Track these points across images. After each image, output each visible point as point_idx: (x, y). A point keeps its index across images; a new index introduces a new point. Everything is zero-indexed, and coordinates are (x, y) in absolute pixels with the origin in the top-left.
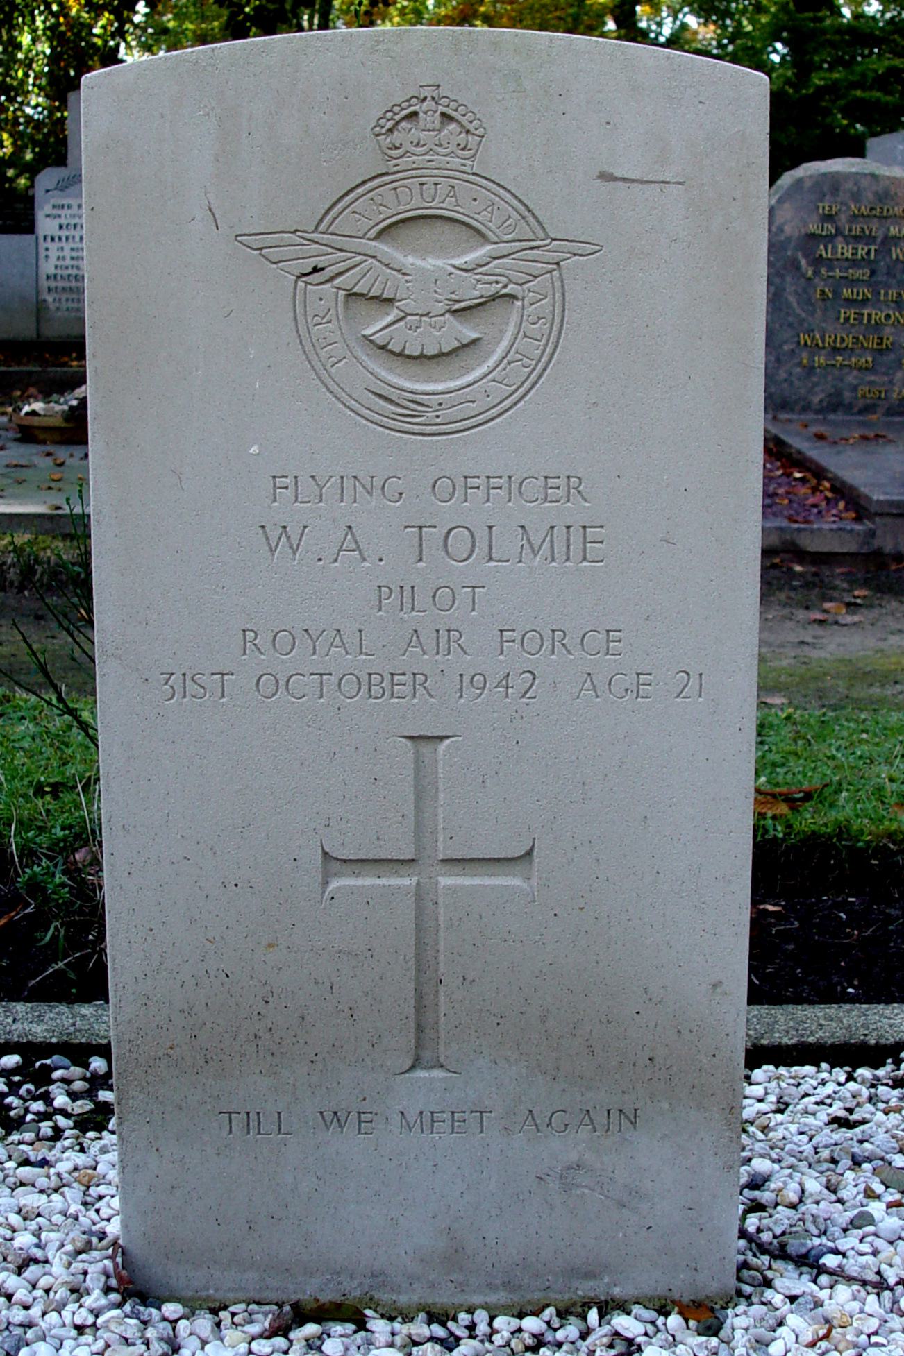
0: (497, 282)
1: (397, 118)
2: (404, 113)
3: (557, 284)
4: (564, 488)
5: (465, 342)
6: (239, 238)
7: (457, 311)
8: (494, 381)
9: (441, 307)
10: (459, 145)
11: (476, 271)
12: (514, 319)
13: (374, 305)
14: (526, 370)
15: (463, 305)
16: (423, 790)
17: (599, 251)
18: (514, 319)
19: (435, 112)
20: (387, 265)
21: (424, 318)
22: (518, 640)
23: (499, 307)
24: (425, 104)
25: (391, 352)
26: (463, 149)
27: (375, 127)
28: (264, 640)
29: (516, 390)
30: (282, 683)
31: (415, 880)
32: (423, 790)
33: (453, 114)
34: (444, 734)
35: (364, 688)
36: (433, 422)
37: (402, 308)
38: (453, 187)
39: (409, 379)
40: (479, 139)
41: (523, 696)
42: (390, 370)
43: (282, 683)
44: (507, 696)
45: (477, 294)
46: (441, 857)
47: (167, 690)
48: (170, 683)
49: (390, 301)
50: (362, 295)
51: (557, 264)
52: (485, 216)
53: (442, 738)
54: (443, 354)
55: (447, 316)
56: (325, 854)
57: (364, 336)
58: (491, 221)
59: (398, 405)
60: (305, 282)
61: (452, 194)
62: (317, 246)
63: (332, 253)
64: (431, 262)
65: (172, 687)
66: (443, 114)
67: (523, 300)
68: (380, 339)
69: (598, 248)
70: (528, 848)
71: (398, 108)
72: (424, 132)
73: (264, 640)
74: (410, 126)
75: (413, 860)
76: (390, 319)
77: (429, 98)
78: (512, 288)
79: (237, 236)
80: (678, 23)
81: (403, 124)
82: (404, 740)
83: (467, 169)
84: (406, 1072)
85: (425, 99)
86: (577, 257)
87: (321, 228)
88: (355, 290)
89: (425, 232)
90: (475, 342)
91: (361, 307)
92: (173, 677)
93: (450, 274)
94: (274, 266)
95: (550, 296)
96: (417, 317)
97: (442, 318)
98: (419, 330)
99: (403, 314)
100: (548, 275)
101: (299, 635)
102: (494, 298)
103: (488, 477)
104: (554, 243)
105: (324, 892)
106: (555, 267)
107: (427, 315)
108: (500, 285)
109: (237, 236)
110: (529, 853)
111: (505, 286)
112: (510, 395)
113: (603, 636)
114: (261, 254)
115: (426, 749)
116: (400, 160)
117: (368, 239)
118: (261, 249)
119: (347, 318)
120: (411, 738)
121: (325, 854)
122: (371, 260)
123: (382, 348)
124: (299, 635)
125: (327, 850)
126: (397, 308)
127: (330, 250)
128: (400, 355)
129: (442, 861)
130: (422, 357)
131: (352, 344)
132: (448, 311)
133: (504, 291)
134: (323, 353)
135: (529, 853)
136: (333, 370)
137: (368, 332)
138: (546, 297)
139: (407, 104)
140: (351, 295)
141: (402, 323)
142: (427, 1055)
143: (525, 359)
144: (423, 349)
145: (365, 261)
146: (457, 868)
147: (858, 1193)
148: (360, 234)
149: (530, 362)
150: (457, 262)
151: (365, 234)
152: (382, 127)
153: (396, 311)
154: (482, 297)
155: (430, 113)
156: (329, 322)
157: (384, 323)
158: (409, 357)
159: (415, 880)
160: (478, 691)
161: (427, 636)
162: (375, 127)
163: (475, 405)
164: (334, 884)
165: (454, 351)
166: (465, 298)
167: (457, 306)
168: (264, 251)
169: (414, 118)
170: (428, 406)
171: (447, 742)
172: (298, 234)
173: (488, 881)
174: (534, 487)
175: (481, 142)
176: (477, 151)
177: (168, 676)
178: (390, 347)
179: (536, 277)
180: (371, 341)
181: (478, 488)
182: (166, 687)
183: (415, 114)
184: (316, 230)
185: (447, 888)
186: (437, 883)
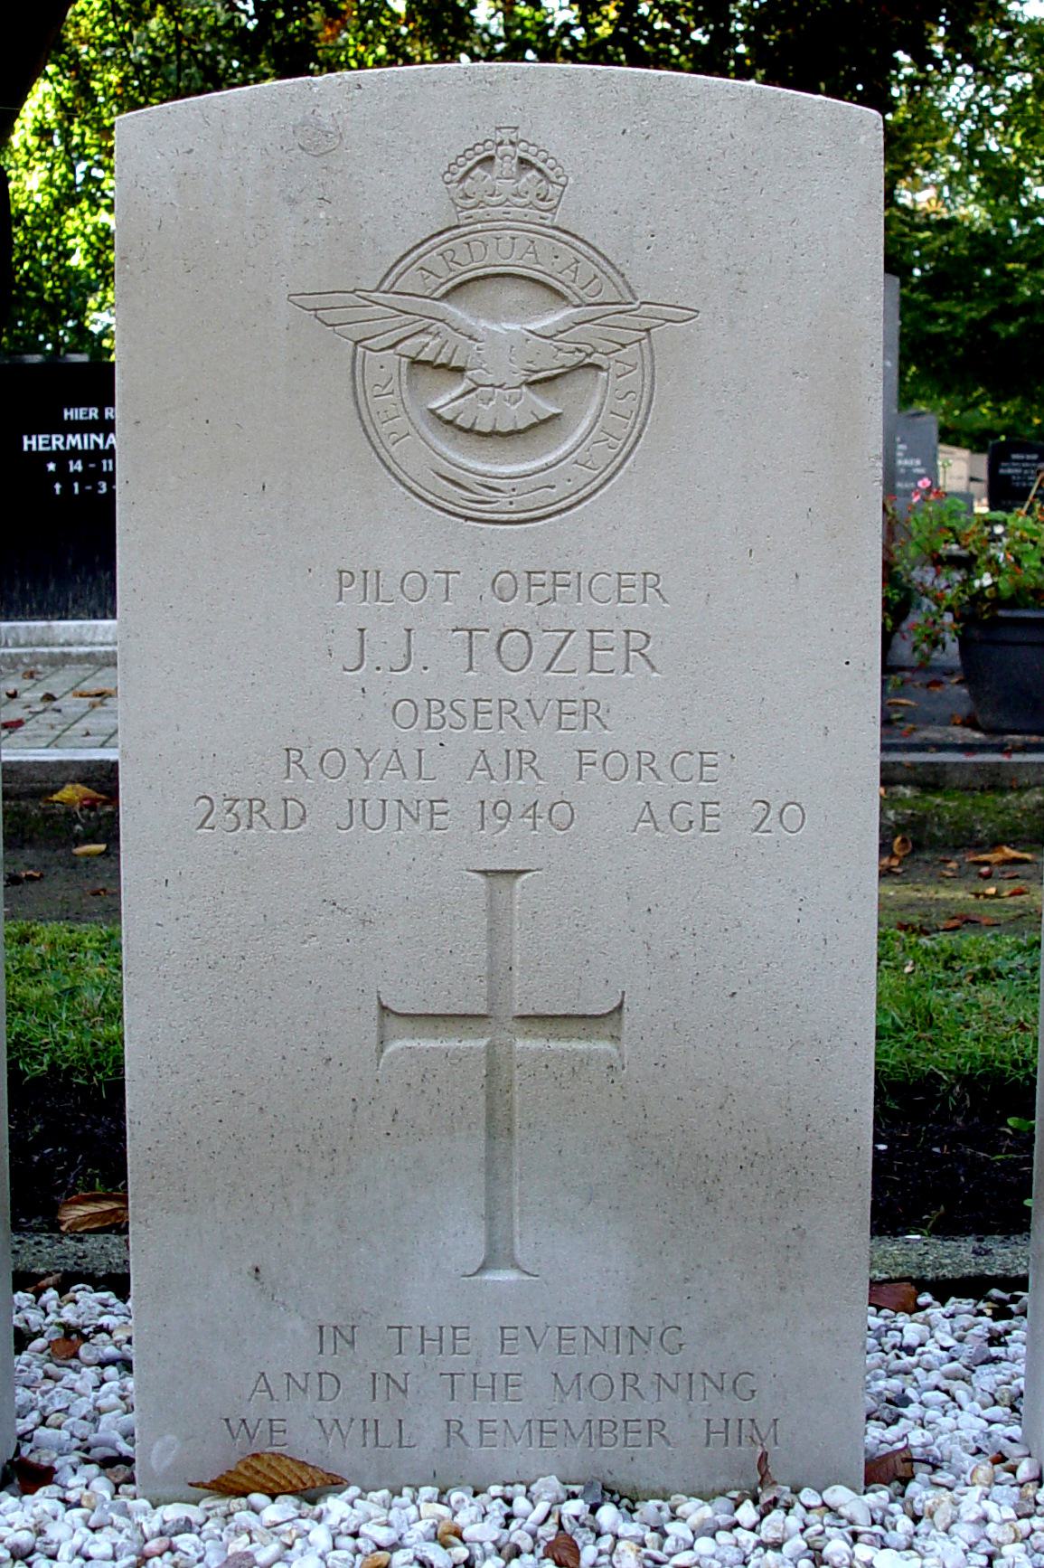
1: (470, 164)
2: (478, 158)
3: (646, 352)
4: (639, 584)
5: (542, 417)
6: (292, 297)
7: (534, 382)
8: (576, 462)
10: (538, 195)
12: (599, 389)
13: (444, 376)
15: (541, 375)
16: (496, 931)
17: (694, 317)
18: (599, 389)
19: (513, 158)
20: (456, 330)
21: (497, 390)
25: (461, 429)
26: (543, 200)
27: (446, 173)
29: (600, 473)
31: (483, 1043)
32: (496, 931)
33: (533, 160)
34: (520, 868)
36: (504, 509)
37: (475, 379)
39: (517, 462)
40: (561, 188)
42: (459, 449)
44: (535, 828)
45: (558, 364)
49: (460, 370)
51: (648, 330)
52: (566, 274)
54: (519, 432)
55: (524, 389)
56: (384, 1008)
57: (432, 411)
58: (574, 281)
59: (471, 492)
60: (364, 347)
61: (531, 249)
65: (235, 815)
66: (522, 161)
67: (607, 370)
68: (446, 413)
69: (695, 314)
70: (615, 1005)
71: (463, 159)
72: (502, 179)
73: (309, 761)
74: (485, 174)
75: (484, 1016)
76: (459, 391)
80: (23, 224)
82: (476, 876)
83: (547, 222)
84: (474, 1274)
86: (668, 324)
87: (382, 289)
88: (422, 357)
90: (556, 416)
91: (427, 376)
93: (527, 340)
96: (490, 389)
97: (518, 390)
99: (473, 386)
102: (580, 367)
103: (555, 573)
106: (644, 334)
107: (500, 387)
108: (583, 354)
110: (620, 1007)
111: (589, 355)
114: (316, 316)
115: (502, 882)
116: (474, 211)
118: (316, 310)
120: (485, 872)
122: (439, 324)
123: (449, 423)
124: (351, 755)
125: (384, 1003)
131: (417, 420)
133: (588, 360)
134: (383, 429)
135: (620, 1007)
136: (393, 449)
137: (434, 405)
139: (471, 152)
140: (415, 362)
144: (516, 423)
146: (536, 1027)
147: (75, 1292)
150: (531, 327)
152: (453, 174)
154: (563, 367)
155: (507, 158)
157: (454, 394)
158: (480, 434)
159: (483, 1043)
160: (503, 822)
162: (446, 173)
163: (554, 490)
164: (392, 1047)
165: (511, 433)
166: (544, 366)
167: (535, 377)
168: (319, 312)
169: (490, 163)
170: (501, 491)
172: (358, 293)
174: (605, 585)
175: (563, 191)
176: (559, 202)
179: (624, 346)
180: (440, 417)
181: (543, 585)
182: (230, 815)
183: (491, 158)
184: (377, 290)
186: (511, 1046)
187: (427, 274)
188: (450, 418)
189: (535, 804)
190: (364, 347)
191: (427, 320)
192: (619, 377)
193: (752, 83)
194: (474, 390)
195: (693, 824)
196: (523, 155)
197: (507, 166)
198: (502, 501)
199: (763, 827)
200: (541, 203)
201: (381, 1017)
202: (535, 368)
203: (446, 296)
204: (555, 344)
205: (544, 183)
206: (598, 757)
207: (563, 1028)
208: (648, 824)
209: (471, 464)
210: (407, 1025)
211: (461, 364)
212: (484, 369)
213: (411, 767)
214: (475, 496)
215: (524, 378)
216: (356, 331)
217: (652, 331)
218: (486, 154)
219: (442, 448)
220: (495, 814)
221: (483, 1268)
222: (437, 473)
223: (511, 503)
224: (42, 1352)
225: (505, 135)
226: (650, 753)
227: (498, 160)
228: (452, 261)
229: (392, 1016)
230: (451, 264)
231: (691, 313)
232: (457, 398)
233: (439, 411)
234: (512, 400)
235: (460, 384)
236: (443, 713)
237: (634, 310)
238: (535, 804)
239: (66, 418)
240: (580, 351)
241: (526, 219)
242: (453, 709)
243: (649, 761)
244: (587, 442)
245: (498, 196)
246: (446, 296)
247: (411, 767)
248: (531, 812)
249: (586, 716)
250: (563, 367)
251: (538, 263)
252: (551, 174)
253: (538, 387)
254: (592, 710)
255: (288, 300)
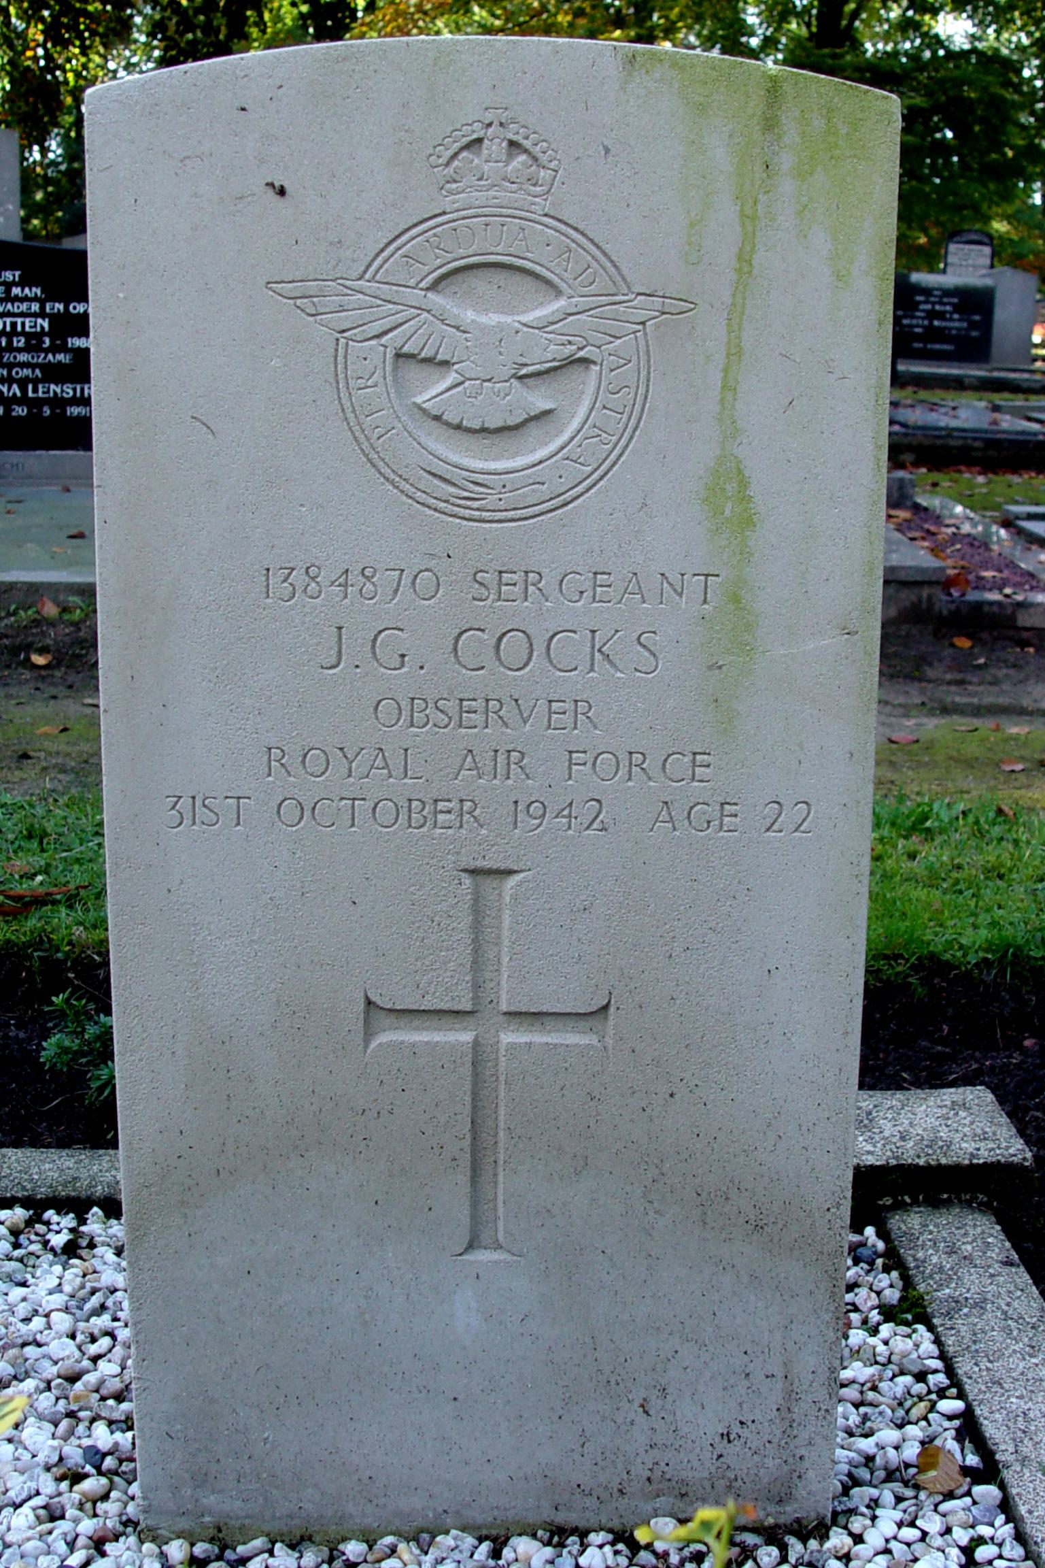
0: (570, 343)
8: (567, 459)
9: (507, 371)
11: (546, 329)
13: (428, 369)
14: (606, 447)
15: (531, 369)
17: (692, 310)
22: (589, 765)
23: (576, 372)
24: (490, 130)
25: (448, 424)
28: (292, 761)
30: (307, 813)
31: (467, 1037)
35: (403, 818)
38: (523, 229)
40: (554, 173)
41: (796, 830)
43: (307, 813)
45: (549, 356)
46: (504, 1007)
47: (173, 815)
48: (177, 807)
49: (446, 364)
50: (412, 356)
51: (643, 323)
53: (510, 872)
56: (369, 1003)
57: (414, 403)
59: (454, 485)
62: (361, 296)
63: (403, 311)
64: (492, 319)
66: (512, 144)
69: (693, 306)
73: (292, 761)
76: (448, 382)
77: (496, 123)
78: (590, 351)
79: (268, 283)
81: (464, 154)
84: (460, 1255)
85: (490, 125)
88: (405, 350)
89: (480, 283)
91: (412, 372)
92: (182, 800)
93: (517, 332)
94: (311, 319)
95: (634, 359)
98: (508, 398)
100: (632, 336)
101: (655, 771)
104: (639, 298)
105: (366, 1047)
106: (640, 327)
108: (575, 347)
109: (268, 283)
110: (606, 1007)
112: (588, 477)
113: (689, 757)
114: (295, 305)
115: (489, 884)
117: (421, 289)
119: (395, 381)
121: (369, 1003)
122: (425, 315)
123: (437, 418)
125: (373, 999)
126: (456, 372)
127: (381, 303)
128: (458, 427)
129: (505, 1014)
130: (483, 430)
132: (514, 376)
133: (581, 354)
135: (606, 1007)
137: (419, 400)
138: (630, 361)
141: (460, 389)
142: (486, 1237)
143: (604, 435)
145: (419, 315)
148: (412, 282)
149: (610, 438)
150: (525, 318)
151: (417, 285)
152: (439, 157)
153: (454, 375)
154: (554, 360)
156: (376, 386)
158: (470, 431)
159: (467, 1037)
161: (485, 760)
167: (524, 371)
169: (477, 146)
170: (488, 487)
171: (513, 881)
172: (339, 281)
173: (437, 1037)
175: (555, 177)
177: (175, 799)
178: (445, 417)
180: (424, 411)
181: (515, 584)
182: (173, 812)
183: (479, 141)
185: (512, 1047)
187: (414, 262)
188: (439, 414)
189: (571, 804)
190: (345, 338)
191: (391, 306)
192: (612, 371)
193: (252, 53)
194: (462, 383)
195: (712, 824)
196: (515, 138)
197: (495, 147)
198: (491, 501)
199: (775, 827)
200: (532, 188)
201: (367, 1013)
202: (524, 360)
203: (433, 287)
204: (545, 335)
205: (534, 167)
206: (589, 757)
207: (550, 1023)
208: (667, 824)
209: (454, 458)
210: (389, 1020)
211: (447, 358)
212: (473, 362)
213: (396, 763)
214: (460, 492)
215: (514, 371)
216: (345, 321)
217: (648, 323)
218: (475, 136)
219: (432, 444)
220: (528, 811)
221: (471, 1246)
222: (429, 473)
223: (500, 500)
224: (950, 1418)
225: (489, 115)
226: (642, 753)
227: (486, 141)
228: (438, 248)
229: (383, 1014)
230: (437, 251)
231: (687, 304)
232: (442, 393)
233: (424, 406)
234: (502, 394)
235: (444, 378)
236: (427, 712)
237: (631, 301)
238: (571, 804)
239: (68, 413)
240: (570, 343)
241: (516, 205)
242: (437, 708)
243: (639, 763)
244: (579, 437)
245: (541, 186)
246: (433, 287)
247: (396, 763)
248: (566, 813)
249: (576, 716)
250: (554, 360)
251: (528, 251)
252: (544, 159)
253: (530, 382)
254: (580, 708)
255: (696, 304)
